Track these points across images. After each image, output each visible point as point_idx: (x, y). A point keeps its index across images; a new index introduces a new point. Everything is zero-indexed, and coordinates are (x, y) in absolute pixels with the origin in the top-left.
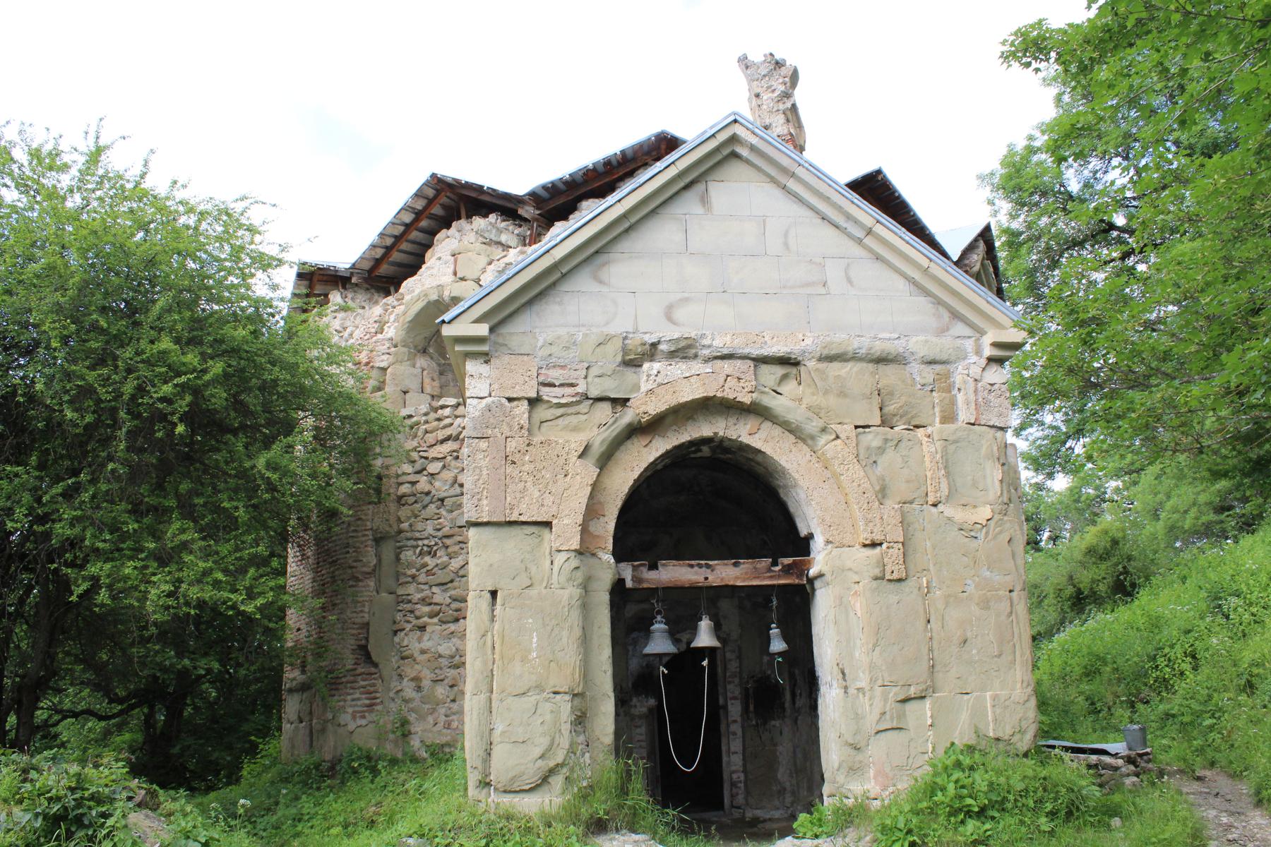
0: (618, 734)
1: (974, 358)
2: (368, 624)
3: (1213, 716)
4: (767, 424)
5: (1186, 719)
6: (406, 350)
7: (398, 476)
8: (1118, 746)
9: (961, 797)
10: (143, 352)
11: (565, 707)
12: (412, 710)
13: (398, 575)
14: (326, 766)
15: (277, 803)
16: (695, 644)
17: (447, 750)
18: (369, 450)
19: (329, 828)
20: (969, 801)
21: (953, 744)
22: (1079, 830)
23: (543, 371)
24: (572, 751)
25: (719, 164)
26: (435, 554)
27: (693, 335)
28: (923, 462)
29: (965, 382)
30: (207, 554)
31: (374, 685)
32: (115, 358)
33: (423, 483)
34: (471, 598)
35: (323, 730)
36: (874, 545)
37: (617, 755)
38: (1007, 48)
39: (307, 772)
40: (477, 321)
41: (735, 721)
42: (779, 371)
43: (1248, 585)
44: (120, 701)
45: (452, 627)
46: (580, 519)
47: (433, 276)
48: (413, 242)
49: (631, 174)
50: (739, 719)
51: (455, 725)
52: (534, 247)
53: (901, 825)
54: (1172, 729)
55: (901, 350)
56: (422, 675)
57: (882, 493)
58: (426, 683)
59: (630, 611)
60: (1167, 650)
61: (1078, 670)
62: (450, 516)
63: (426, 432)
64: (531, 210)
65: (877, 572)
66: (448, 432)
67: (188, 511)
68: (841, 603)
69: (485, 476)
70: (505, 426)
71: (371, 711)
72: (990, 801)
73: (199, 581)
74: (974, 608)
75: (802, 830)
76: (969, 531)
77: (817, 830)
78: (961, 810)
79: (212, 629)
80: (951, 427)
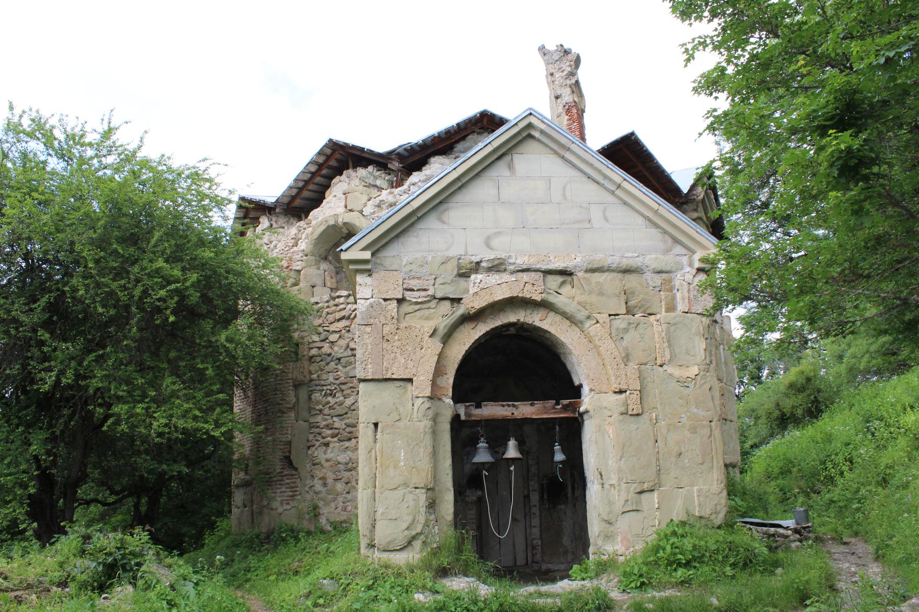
0: (456, 514)
1: (688, 269)
2: (290, 442)
3: (859, 502)
4: (552, 314)
5: (841, 504)
6: (313, 258)
7: (310, 343)
8: (790, 523)
9: (675, 554)
10: (146, 268)
12: (321, 499)
13: (310, 409)
14: (263, 536)
15: (233, 561)
17: (344, 525)
19: (268, 576)
20: (680, 556)
21: (672, 520)
22: (751, 575)
24: (426, 525)
26: (335, 395)
28: (654, 338)
30: (188, 399)
32: (128, 272)
33: (326, 348)
34: (361, 427)
35: (261, 513)
36: (621, 392)
37: (456, 528)
38: (696, 85)
39: (251, 540)
40: (364, 249)
41: (535, 506)
42: (560, 279)
43: (888, 412)
44: (117, 493)
45: (347, 444)
46: (431, 377)
47: (332, 209)
48: (318, 184)
50: (537, 504)
51: (349, 508)
52: (399, 189)
53: (636, 571)
55: (640, 264)
56: (327, 475)
57: (627, 358)
58: (330, 481)
59: (464, 435)
60: (833, 457)
61: (776, 470)
62: (344, 370)
63: (328, 313)
64: (397, 164)
65: (623, 409)
66: (343, 313)
67: (175, 372)
68: (599, 429)
72: (693, 556)
73: (184, 416)
74: (686, 432)
75: (574, 575)
76: (683, 382)
77: (584, 575)
78: (674, 562)
79: (196, 449)
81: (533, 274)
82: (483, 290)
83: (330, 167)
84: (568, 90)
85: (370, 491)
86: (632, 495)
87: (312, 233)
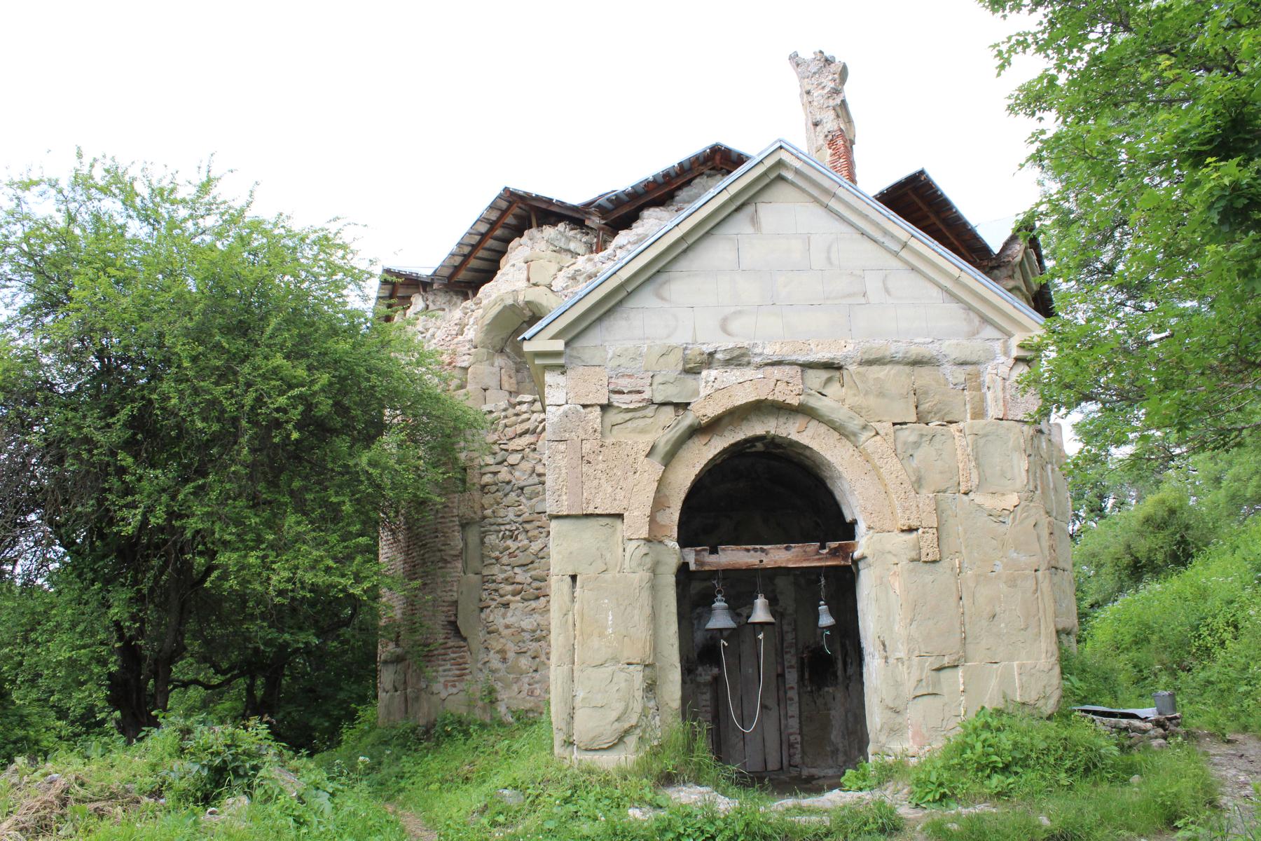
0: (684, 699)
1: (1002, 359)
3: (1248, 684)
4: (814, 423)
5: (1223, 686)
6: (484, 350)
8: (1150, 712)
10: (259, 368)
11: (638, 677)
14: (420, 730)
15: (380, 763)
16: (751, 620)
18: (453, 444)
20: (994, 758)
21: (983, 708)
22: (1095, 784)
23: (613, 380)
24: (644, 714)
25: (767, 186)
27: (745, 345)
29: (994, 381)
30: (318, 544)
31: (463, 657)
32: (235, 373)
33: (504, 474)
35: (417, 699)
36: (911, 530)
37: (684, 718)
38: (1012, 101)
39: (405, 736)
40: (554, 337)
42: (824, 375)
44: (224, 673)
45: (533, 604)
46: (648, 512)
50: (796, 686)
51: (537, 692)
53: (933, 779)
54: (1209, 696)
55: (935, 353)
56: (507, 648)
57: (918, 483)
58: (511, 655)
59: (694, 591)
60: (1209, 620)
65: (914, 554)
66: (526, 426)
68: (882, 583)
69: (564, 475)
70: (580, 430)
71: (462, 681)
72: (1014, 758)
73: (313, 568)
75: (848, 784)
76: (998, 517)
77: (860, 783)
79: (330, 612)
80: (981, 422)
81: (787, 368)
82: (718, 391)
83: (506, 226)
84: (832, 114)
86: (927, 673)
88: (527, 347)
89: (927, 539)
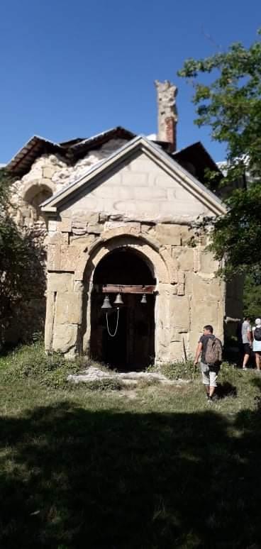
36: (174, 284)
40: (53, 206)
49: (107, 141)
65: (175, 292)
68: (163, 301)
82: (111, 230)
83: (34, 152)
84: (169, 109)
85: (51, 324)
86: (176, 334)
87: (24, 188)
88: (43, 209)
89: (180, 289)
